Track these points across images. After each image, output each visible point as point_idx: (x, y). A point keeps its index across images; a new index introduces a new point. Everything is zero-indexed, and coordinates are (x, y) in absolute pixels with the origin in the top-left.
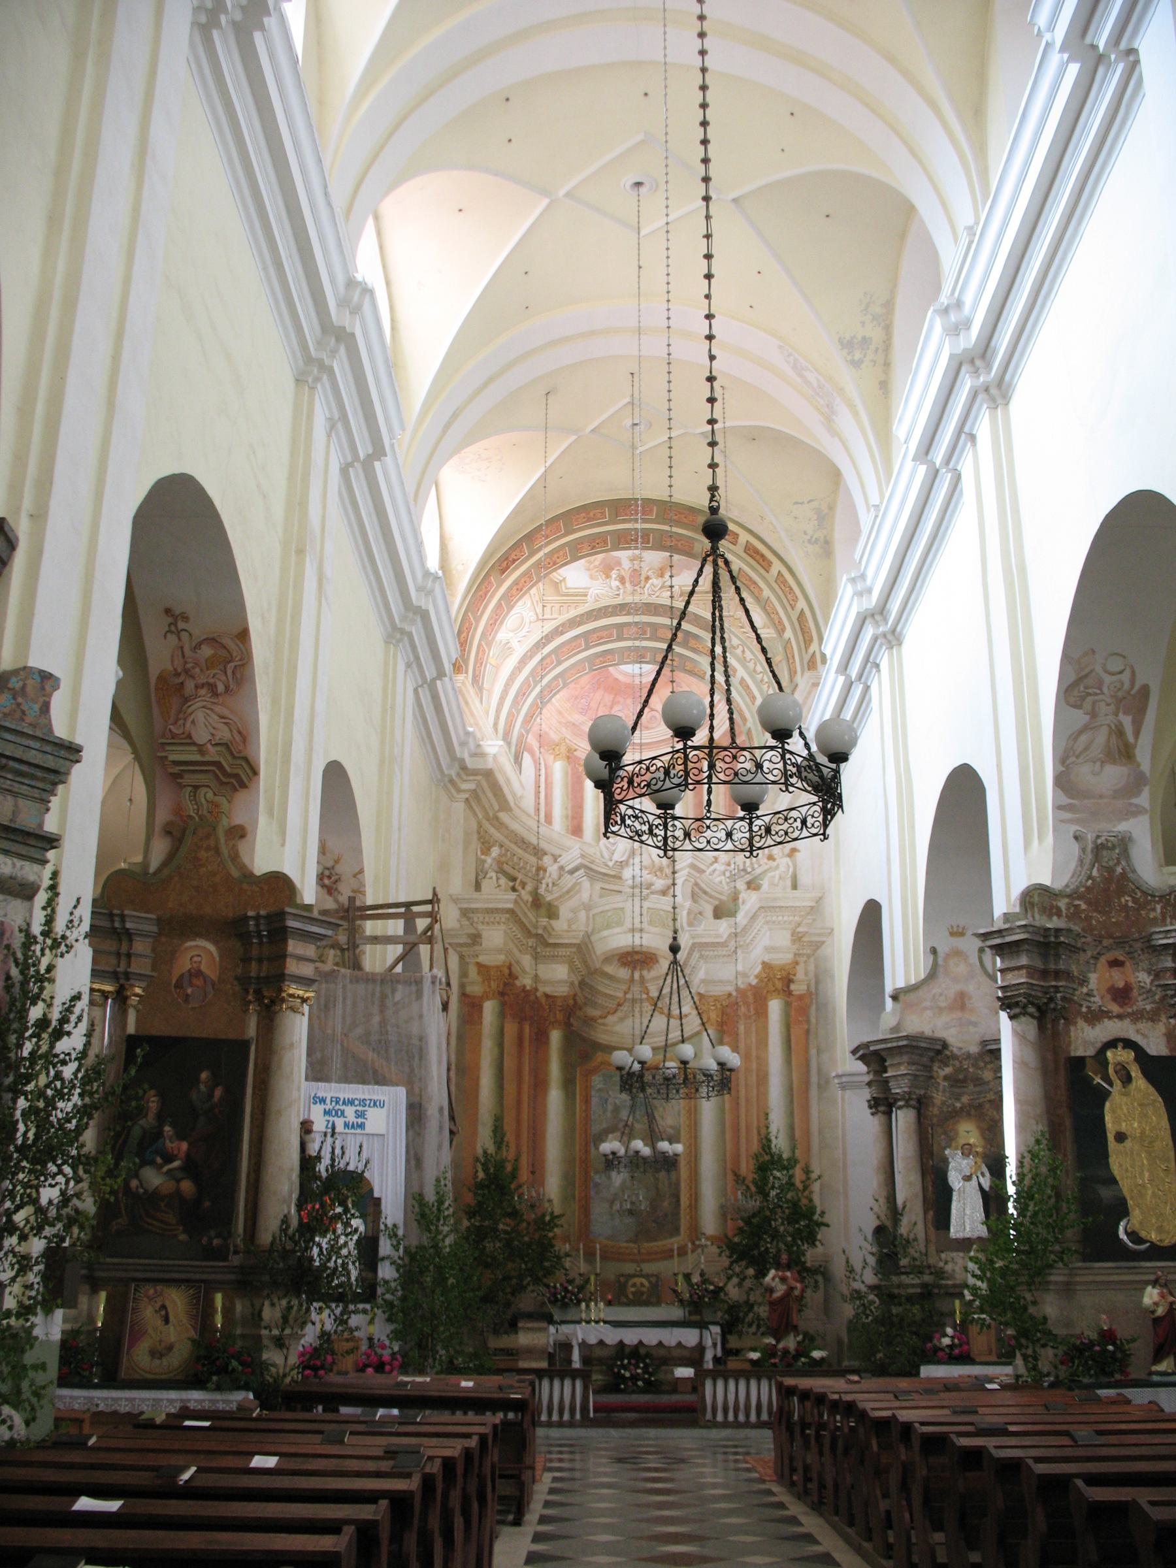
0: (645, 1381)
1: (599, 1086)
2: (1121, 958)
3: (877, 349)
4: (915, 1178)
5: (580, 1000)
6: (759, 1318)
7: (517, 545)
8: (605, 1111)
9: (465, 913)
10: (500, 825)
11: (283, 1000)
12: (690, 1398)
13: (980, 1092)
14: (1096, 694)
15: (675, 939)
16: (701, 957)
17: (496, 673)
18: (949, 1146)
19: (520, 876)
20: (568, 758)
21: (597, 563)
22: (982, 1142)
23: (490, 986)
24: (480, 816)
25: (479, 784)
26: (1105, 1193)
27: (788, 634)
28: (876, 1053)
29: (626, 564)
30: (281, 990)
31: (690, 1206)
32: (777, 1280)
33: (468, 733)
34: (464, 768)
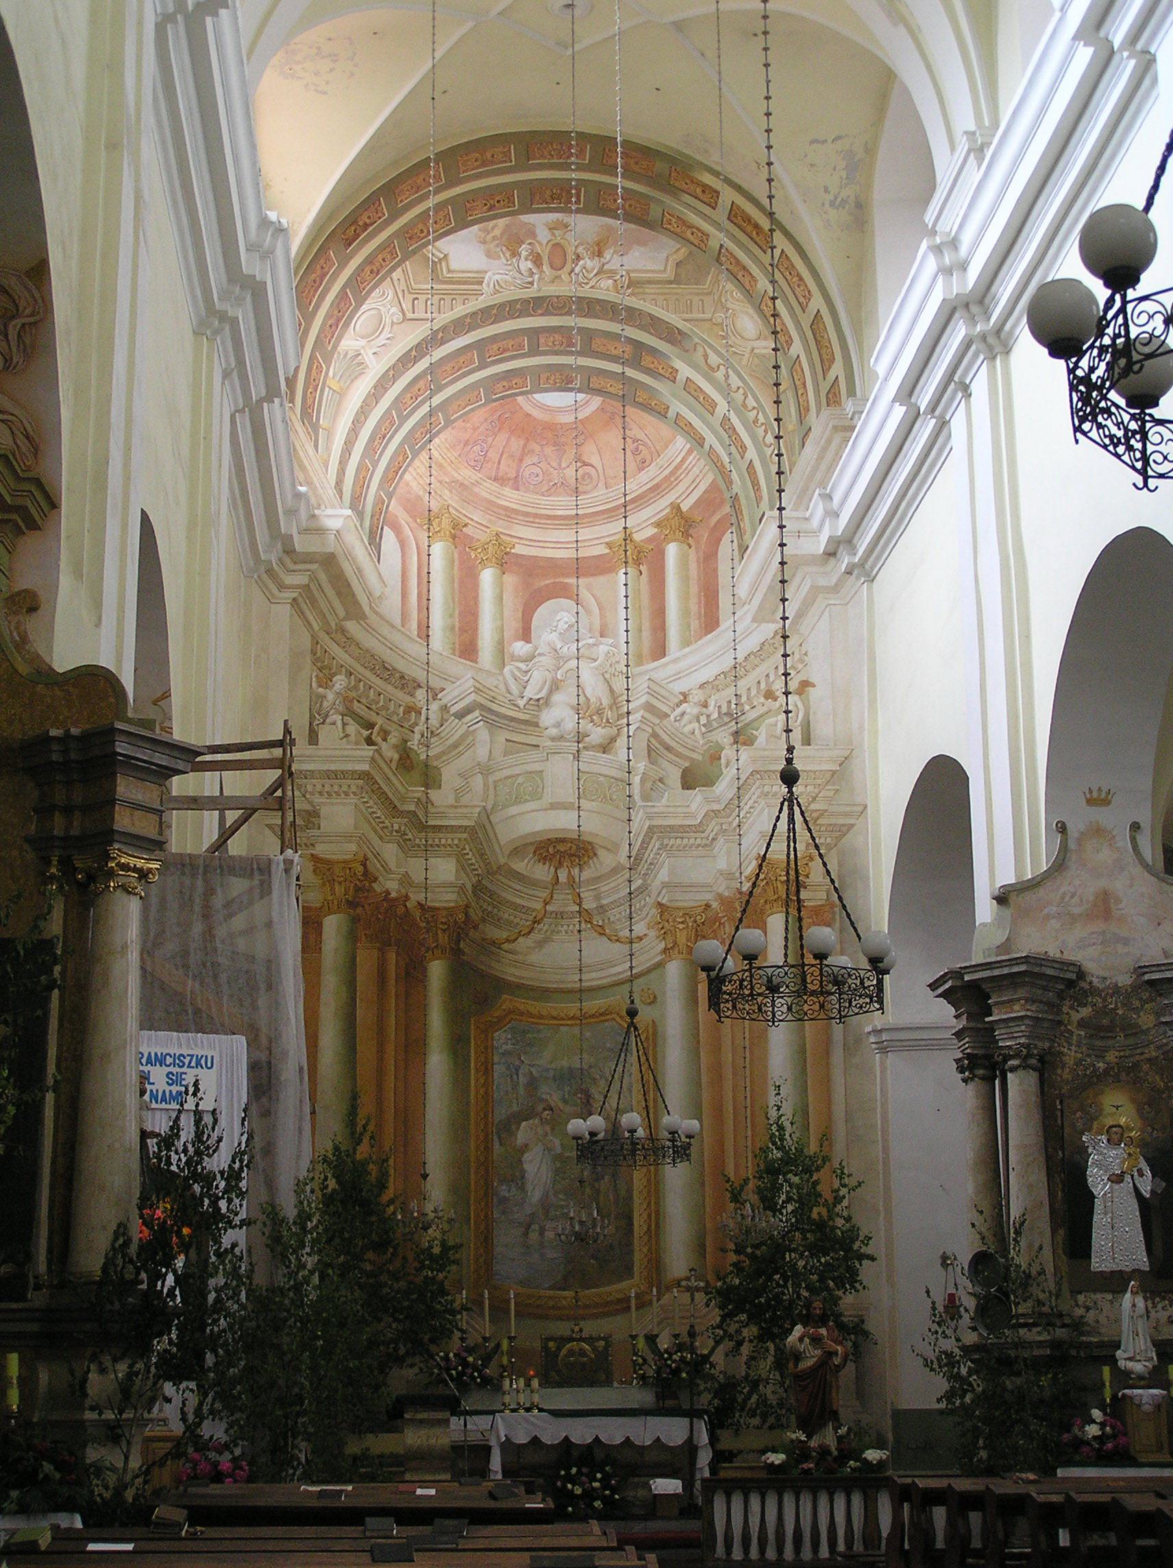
0: (605, 1500)
1: (504, 1047)
4: (1039, 1177)
5: (475, 915)
6: (763, 1401)
7: (370, 202)
10: (348, 641)
11: (111, 874)
12: (690, 1526)
15: (789, 761)
16: (663, 847)
17: (339, 404)
19: (380, 721)
20: (454, 537)
21: (497, 232)
23: (333, 893)
24: (316, 627)
25: (314, 578)
27: (797, 348)
28: (974, 985)
29: (543, 235)
32: (807, 1340)
33: (298, 496)
34: (289, 551)
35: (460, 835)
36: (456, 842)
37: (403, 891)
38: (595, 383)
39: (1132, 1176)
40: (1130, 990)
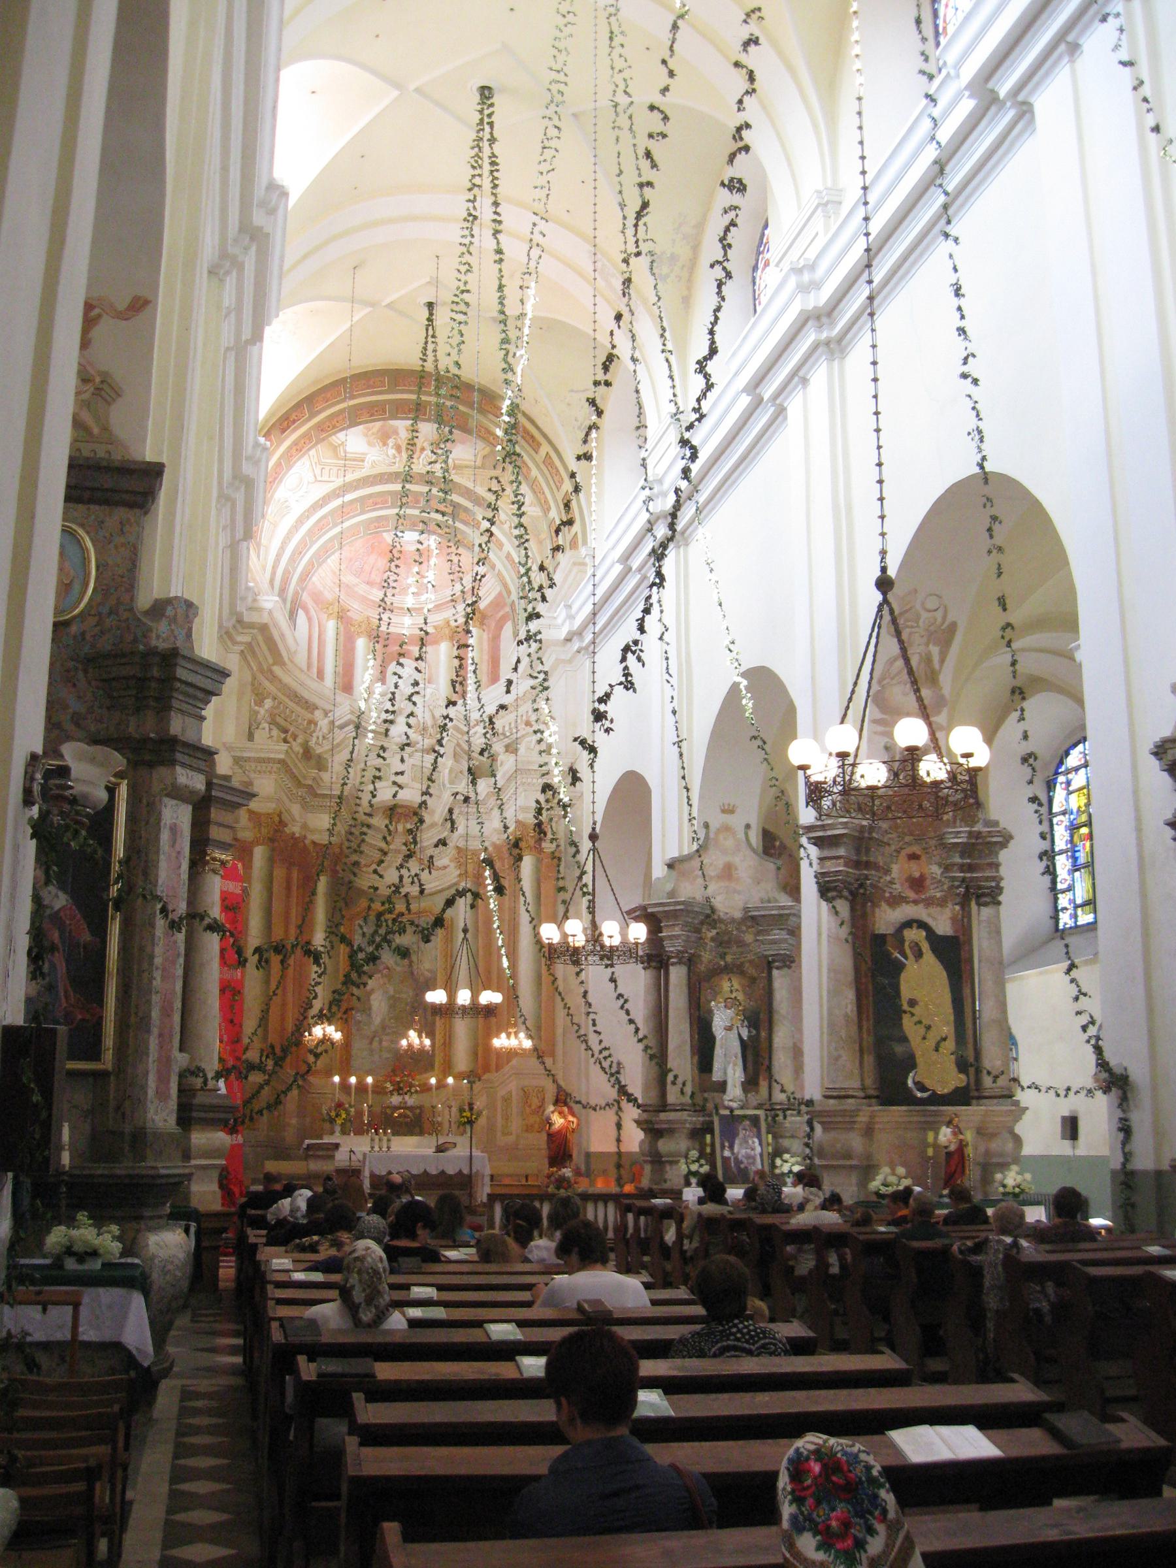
2: (918, 853)
3: (683, 266)
7: (298, 406)
9: (237, 761)
10: (274, 678)
11: (207, 863)
13: (742, 953)
14: (912, 627)
19: (292, 729)
21: (375, 430)
25: (254, 638)
26: (899, 1049)
30: (206, 854)
31: (444, 1044)
34: (240, 621)
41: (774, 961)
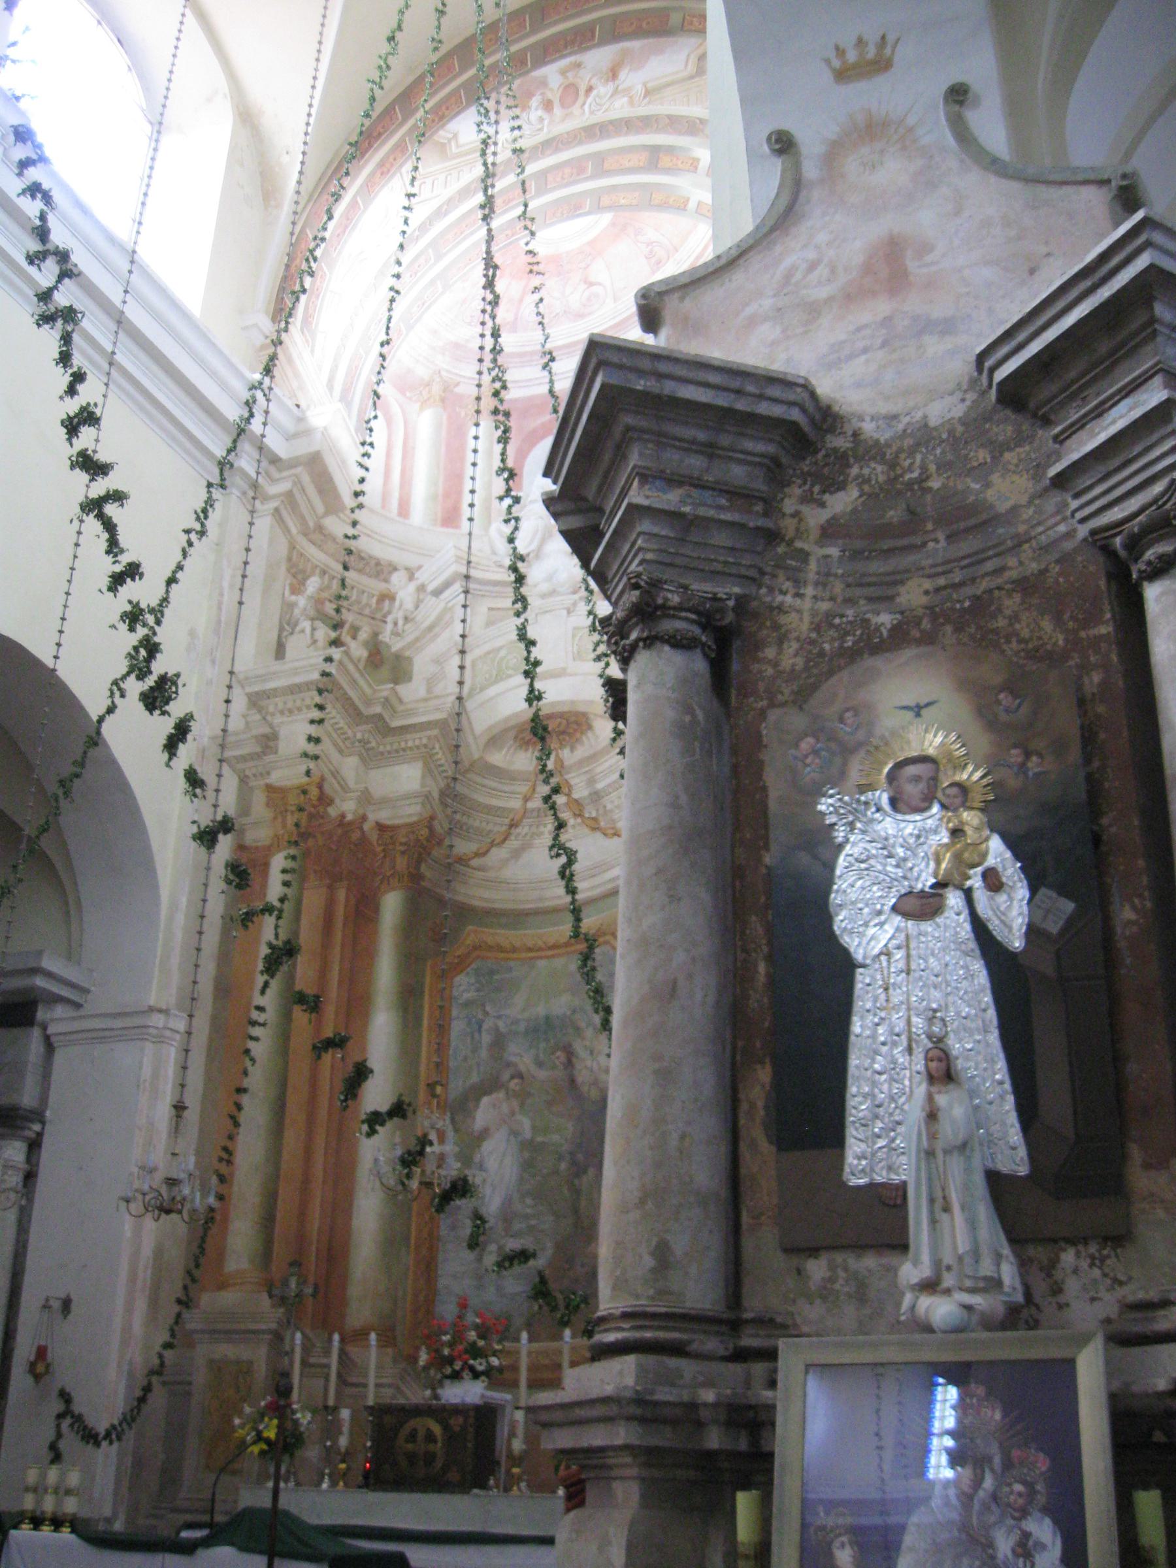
1: (466, 996)
5: (440, 827)
8: (475, 1050)
18: (837, 779)
20: (443, 400)
22: (983, 742)
24: (294, 530)
25: (298, 482)
35: (429, 733)
36: (425, 741)
37: (361, 812)
38: (606, 201)
39: (968, 894)
40: (960, 429)
41: (1136, 544)
